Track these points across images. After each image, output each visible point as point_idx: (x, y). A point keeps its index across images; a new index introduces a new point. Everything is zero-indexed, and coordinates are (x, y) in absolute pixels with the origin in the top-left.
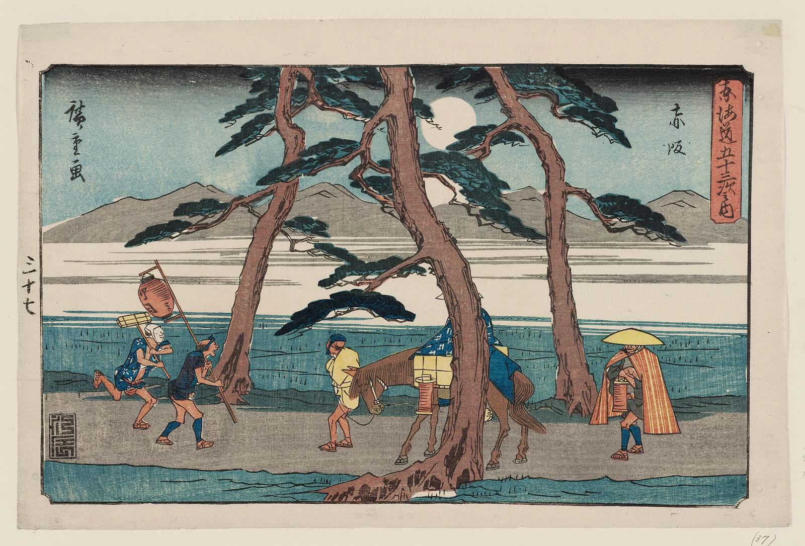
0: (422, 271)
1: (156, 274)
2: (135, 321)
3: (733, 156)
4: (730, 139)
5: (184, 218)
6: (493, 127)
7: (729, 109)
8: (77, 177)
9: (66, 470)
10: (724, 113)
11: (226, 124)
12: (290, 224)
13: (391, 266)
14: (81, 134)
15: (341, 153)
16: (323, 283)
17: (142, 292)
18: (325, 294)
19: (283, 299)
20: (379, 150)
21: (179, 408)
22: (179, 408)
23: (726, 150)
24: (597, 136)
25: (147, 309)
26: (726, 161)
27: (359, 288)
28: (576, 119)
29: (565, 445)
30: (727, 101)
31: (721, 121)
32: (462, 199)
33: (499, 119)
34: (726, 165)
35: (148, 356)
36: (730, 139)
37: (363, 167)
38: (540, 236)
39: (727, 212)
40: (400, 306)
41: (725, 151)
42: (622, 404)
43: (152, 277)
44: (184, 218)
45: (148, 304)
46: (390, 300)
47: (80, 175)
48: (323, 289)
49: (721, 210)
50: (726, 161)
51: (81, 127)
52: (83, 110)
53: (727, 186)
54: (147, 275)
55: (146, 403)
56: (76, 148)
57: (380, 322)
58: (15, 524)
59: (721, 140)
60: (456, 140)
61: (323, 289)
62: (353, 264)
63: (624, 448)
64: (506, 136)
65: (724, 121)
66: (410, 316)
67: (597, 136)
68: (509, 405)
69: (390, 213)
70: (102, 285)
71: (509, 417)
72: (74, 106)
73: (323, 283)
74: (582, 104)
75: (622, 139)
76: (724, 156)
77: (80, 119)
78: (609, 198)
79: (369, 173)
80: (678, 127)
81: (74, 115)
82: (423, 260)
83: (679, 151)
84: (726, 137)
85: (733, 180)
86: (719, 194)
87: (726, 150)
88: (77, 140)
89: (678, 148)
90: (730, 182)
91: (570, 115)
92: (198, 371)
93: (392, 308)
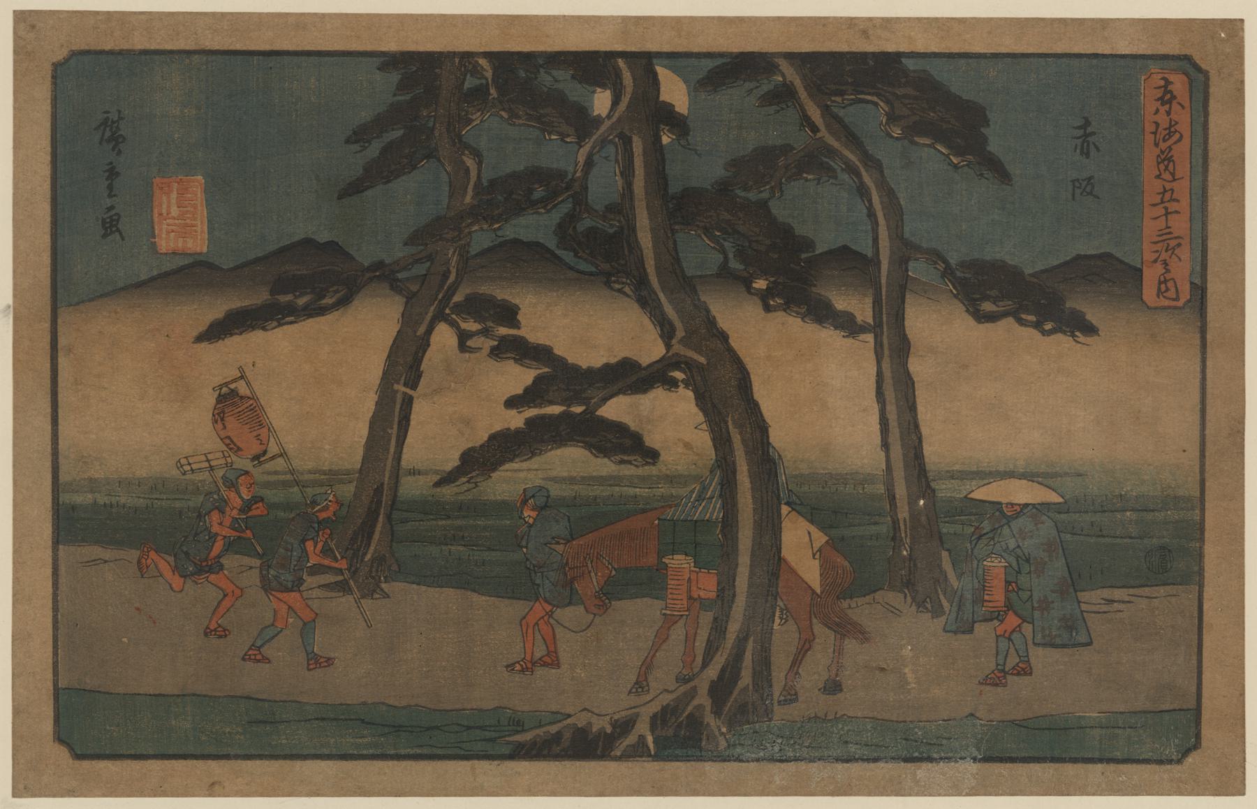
0: (672, 384)
1: (242, 388)
4: (1173, 174)
5: (285, 299)
7: (1171, 126)
8: (112, 232)
10: (1162, 133)
12: (458, 308)
13: (627, 376)
15: (539, 193)
16: (512, 403)
17: (219, 417)
18: (516, 420)
19: (438, 433)
23: (1165, 191)
25: (227, 445)
26: (1166, 208)
29: (910, 653)
30: (1168, 113)
31: (1157, 145)
32: (735, 265)
35: (227, 522)
36: (1173, 174)
37: (571, 218)
38: (863, 329)
39: (1167, 290)
42: (997, 598)
43: (234, 393)
44: (285, 299)
45: (228, 437)
46: (620, 428)
47: (118, 230)
49: (1159, 289)
50: (1166, 208)
53: (1167, 251)
54: (225, 390)
55: (225, 596)
56: (110, 187)
57: (605, 466)
59: (1158, 177)
60: (175, 473)
61: (514, 412)
62: (558, 377)
64: (814, 162)
65: (1163, 146)
66: (652, 456)
69: (619, 291)
73: (512, 403)
75: (996, 168)
76: (1162, 202)
79: (586, 223)
81: (108, 134)
82: (676, 365)
86: (1155, 261)
87: (1165, 191)
88: (112, 173)
89: (1088, 189)
90: (1173, 243)
91: (915, 129)
93: (626, 443)
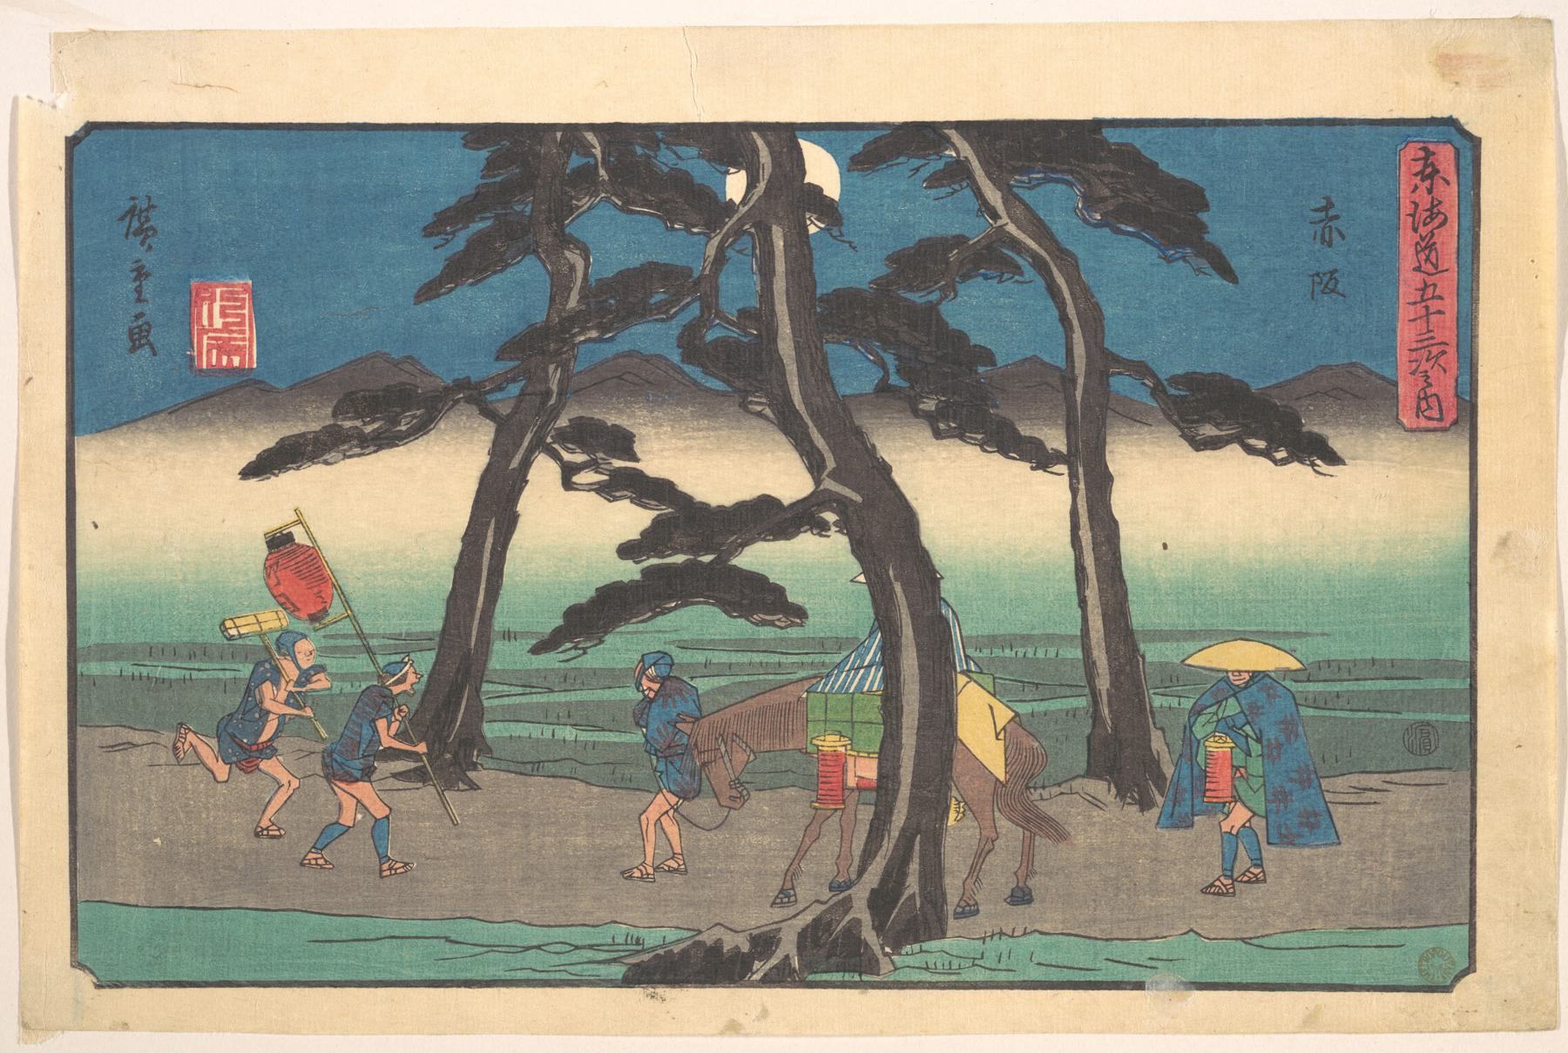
0: (821, 528)
1: (300, 536)
2: (256, 628)
3: (1441, 298)
6: (960, 240)
9: (132, 927)
11: (436, 240)
12: (563, 437)
13: (768, 518)
14: (149, 260)
18: (630, 571)
20: (737, 288)
21: (345, 798)
22: (345, 798)
24: (1169, 262)
27: (695, 551)
28: (1123, 227)
33: (975, 229)
34: (1427, 315)
35: (282, 695)
40: (779, 591)
41: (1423, 290)
48: (629, 564)
50: (1427, 307)
51: (150, 247)
52: (152, 214)
58: (14, 1027)
63: (1228, 872)
64: (993, 257)
65: (1423, 231)
67: (1169, 262)
68: (550, 262)
70: (79, 487)
71: (997, 814)
72: (134, 207)
73: (627, 551)
74: (1138, 197)
77: (144, 233)
78: (1191, 381)
80: (1330, 245)
83: (1332, 291)
84: (1428, 259)
85: (1443, 347)
92: (381, 724)
93: (761, 598)
